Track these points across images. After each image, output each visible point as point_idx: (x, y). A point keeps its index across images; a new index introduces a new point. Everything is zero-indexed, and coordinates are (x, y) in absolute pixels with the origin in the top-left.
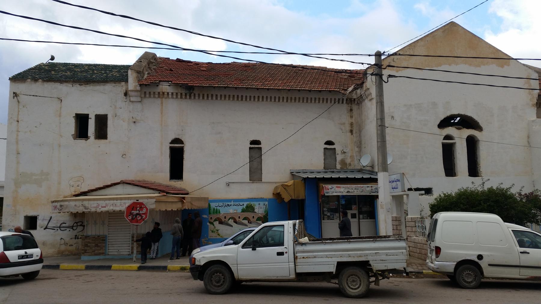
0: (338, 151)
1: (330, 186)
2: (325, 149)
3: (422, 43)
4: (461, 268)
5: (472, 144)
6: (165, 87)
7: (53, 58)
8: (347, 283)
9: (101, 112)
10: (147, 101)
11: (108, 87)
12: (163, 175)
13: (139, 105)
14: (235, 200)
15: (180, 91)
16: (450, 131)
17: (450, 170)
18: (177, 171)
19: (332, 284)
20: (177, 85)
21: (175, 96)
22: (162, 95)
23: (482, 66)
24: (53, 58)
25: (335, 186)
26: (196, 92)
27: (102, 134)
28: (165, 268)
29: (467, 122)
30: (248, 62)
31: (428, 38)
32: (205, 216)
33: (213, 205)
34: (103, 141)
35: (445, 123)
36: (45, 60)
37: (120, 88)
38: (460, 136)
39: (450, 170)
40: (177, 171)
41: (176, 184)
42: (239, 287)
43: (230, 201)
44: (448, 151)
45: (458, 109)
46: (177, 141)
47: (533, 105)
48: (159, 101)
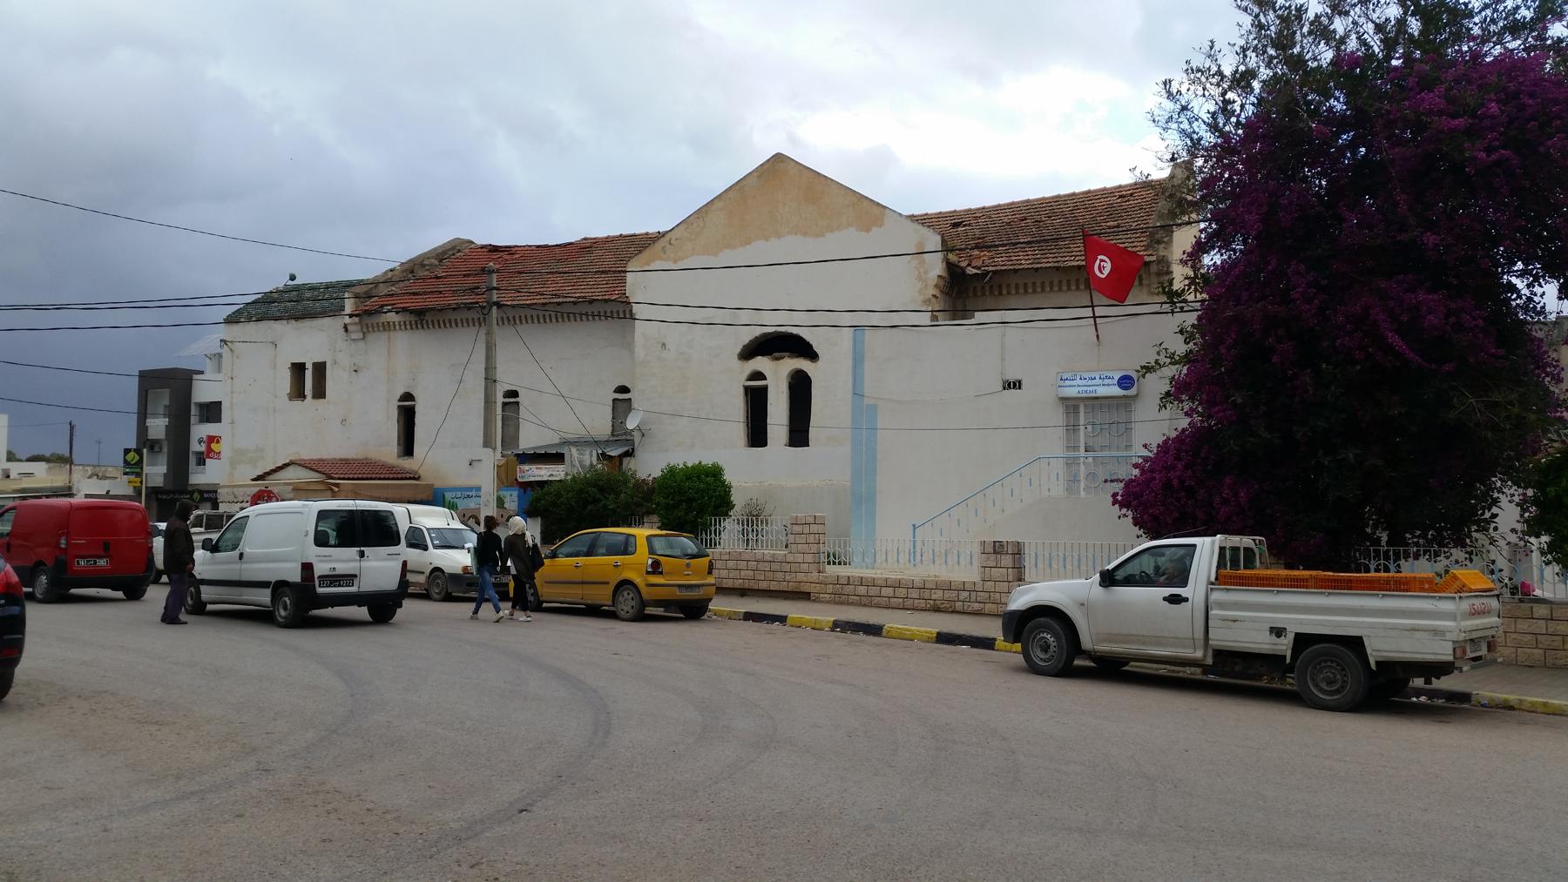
1: (526, 467)
2: (615, 400)
3: (719, 204)
5: (800, 388)
6: (392, 317)
7: (293, 278)
8: (1317, 686)
10: (370, 337)
11: (327, 321)
13: (362, 344)
15: (408, 317)
16: (761, 363)
17: (757, 435)
19: (1291, 683)
21: (404, 326)
22: (388, 327)
24: (293, 278)
25: (533, 467)
26: (429, 317)
27: (320, 393)
28: (874, 630)
29: (801, 348)
30: (727, 257)
31: (731, 194)
35: (749, 353)
36: (281, 282)
38: (777, 373)
39: (757, 435)
40: (407, 447)
44: (756, 399)
45: (774, 322)
46: (408, 396)
48: (384, 336)
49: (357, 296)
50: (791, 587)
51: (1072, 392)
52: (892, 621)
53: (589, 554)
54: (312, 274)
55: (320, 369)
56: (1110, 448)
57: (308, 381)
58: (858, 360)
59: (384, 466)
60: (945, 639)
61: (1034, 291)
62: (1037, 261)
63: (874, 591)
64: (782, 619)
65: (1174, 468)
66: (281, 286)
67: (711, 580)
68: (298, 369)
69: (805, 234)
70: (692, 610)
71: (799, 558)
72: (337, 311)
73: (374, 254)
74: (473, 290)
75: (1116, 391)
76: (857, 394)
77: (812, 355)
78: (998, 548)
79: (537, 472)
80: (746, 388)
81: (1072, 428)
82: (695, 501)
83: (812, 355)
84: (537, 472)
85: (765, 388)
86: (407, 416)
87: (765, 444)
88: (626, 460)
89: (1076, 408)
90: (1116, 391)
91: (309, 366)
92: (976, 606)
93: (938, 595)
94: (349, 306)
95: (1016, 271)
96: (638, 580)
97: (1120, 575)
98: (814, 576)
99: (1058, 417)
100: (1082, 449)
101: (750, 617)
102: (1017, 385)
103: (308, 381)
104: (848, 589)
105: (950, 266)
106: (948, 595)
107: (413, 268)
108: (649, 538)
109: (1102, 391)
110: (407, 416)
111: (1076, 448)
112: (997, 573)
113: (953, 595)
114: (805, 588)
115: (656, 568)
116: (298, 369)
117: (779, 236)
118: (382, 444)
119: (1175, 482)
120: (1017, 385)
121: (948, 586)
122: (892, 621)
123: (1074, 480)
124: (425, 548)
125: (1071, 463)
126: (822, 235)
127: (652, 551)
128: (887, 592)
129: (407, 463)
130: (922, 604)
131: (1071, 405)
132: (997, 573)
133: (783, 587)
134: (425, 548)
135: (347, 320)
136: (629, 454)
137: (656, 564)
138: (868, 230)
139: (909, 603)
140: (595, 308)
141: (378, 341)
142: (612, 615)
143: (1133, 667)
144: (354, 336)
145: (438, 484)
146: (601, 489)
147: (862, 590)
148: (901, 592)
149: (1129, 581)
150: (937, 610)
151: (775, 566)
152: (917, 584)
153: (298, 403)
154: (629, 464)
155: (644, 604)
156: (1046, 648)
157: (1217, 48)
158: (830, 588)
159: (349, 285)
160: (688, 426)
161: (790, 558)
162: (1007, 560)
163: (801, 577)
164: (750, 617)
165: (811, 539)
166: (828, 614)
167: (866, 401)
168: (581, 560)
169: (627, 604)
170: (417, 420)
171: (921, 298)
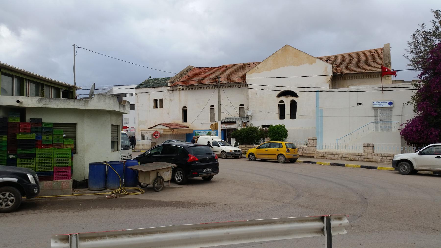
0: (245, 108)
4: (406, 163)
5: (293, 105)
6: (181, 87)
7: (150, 77)
9: (161, 98)
10: (175, 92)
12: (180, 121)
13: (172, 94)
14: (204, 130)
15: (184, 87)
16: (282, 98)
18: (185, 120)
20: (183, 86)
22: (179, 90)
23: (301, 65)
24: (150, 77)
26: (190, 87)
27: (162, 106)
29: (293, 94)
32: (194, 136)
33: (196, 132)
34: (162, 109)
35: (279, 96)
36: (147, 78)
37: (165, 89)
38: (287, 101)
40: (185, 120)
41: (185, 124)
42: (413, 172)
43: (202, 130)
44: (282, 108)
46: (185, 107)
47: (327, 82)
48: (178, 92)
49: (171, 82)
50: (309, 155)
51: (376, 106)
52: (347, 163)
53: (269, 148)
54: (156, 76)
55: (161, 100)
56: (386, 120)
57: (158, 103)
58: (317, 99)
59: (179, 125)
60: (362, 167)
61: (354, 79)
62: (355, 71)
63: (332, 156)
64: (315, 163)
65: (418, 126)
66: (147, 79)
67: (298, 154)
68: (156, 101)
69: (294, 65)
70: (293, 161)
71: (311, 148)
72: (165, 85)
73: (171, 71)
74: (215, 82)
75: (388, 106)
76: (317, 107)
77: (296, 96)
78: (368, 145)
79: (226, 126)
80: (279, 105)
81: (376, 116)
82: (279, 134)
83: (296, 96)
84: (226, 126)
85: (284, 105)
86: (185, 112)
87: (284, 118)
88: (247, 123)
89: (377, 110)
90: (388, 106)
91: (158, 100)
92: (362, 159)
93: (351, 156)
94: (169, 85)
95: (350, 74)
96: (284, 154)
97: (261, 147)
98: (315, 152)
99: (372, 113)
100: (379, 120)
101: (305, 162)
102: (361, 104)
103: (158, 103)
104: (325, 155)
105: (333, 72)
106: (354, 157)
107: (181, 74)
108: (285, 144)
109: (384, 106)
110: (185, 112)
111: (378, 120)
112: (368, 151)
113: (356, 157)
114: (313, 155)
115: (288, 151)
116: (156, 101)
117: (287, 66)
118: (178, 119)
119: (419, 130)
120: (361, 104)
121: (354, 155)
122: (347, 163)
123: (376, 128)
124: (219, 146)
125: (376, 123)
126: (299, 65)
127: (287, 147)
128: (337, 156)
129: (185, 124)
130: (347, 159)
131: (376, 109)
132: (368, 151)
133: (306, 155)
134: (219, 146)
135: (169, 88)
136: (248, 121)
137: (288, 150)
138: (312, 64)
139: (343, 159)
140: (231, 84)
141: (177, 93)
142: (278, 162)
143: (419, 172)
144: (170, 92)
145: (194, 129)
146: (253, 131)
147: (329, 156)
148: (341, 156)
149: (424, 154)
150: (351, 160)
151: (304, 150)
152: (345, 154)
153: (156, 109)
154: (248, 124)
155: (286, 159)
156: (404, 169)
157: (424, 25)
158: (320, 155)
159: (169, 79)
160: (264, 116)
161: (308, 148)
162: (371, 148)
163: (311, 152)
164: (305, 162)
165: (314, 143)
166: (328, 162)
167: (320, 109)
168: (268, 149)
169: (281, 159)
170: (187, 113)
171: (326, 81)
